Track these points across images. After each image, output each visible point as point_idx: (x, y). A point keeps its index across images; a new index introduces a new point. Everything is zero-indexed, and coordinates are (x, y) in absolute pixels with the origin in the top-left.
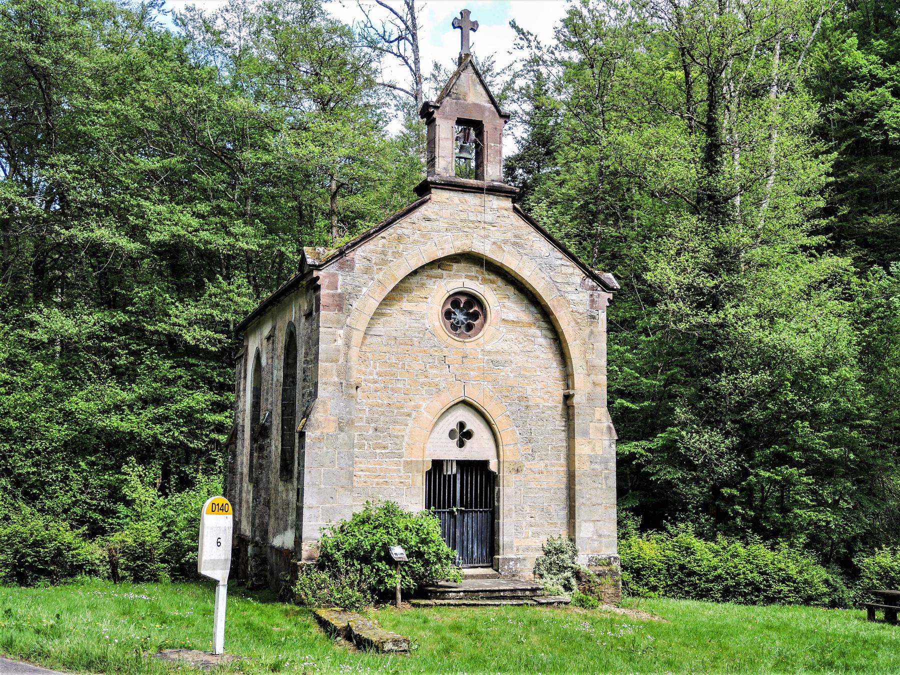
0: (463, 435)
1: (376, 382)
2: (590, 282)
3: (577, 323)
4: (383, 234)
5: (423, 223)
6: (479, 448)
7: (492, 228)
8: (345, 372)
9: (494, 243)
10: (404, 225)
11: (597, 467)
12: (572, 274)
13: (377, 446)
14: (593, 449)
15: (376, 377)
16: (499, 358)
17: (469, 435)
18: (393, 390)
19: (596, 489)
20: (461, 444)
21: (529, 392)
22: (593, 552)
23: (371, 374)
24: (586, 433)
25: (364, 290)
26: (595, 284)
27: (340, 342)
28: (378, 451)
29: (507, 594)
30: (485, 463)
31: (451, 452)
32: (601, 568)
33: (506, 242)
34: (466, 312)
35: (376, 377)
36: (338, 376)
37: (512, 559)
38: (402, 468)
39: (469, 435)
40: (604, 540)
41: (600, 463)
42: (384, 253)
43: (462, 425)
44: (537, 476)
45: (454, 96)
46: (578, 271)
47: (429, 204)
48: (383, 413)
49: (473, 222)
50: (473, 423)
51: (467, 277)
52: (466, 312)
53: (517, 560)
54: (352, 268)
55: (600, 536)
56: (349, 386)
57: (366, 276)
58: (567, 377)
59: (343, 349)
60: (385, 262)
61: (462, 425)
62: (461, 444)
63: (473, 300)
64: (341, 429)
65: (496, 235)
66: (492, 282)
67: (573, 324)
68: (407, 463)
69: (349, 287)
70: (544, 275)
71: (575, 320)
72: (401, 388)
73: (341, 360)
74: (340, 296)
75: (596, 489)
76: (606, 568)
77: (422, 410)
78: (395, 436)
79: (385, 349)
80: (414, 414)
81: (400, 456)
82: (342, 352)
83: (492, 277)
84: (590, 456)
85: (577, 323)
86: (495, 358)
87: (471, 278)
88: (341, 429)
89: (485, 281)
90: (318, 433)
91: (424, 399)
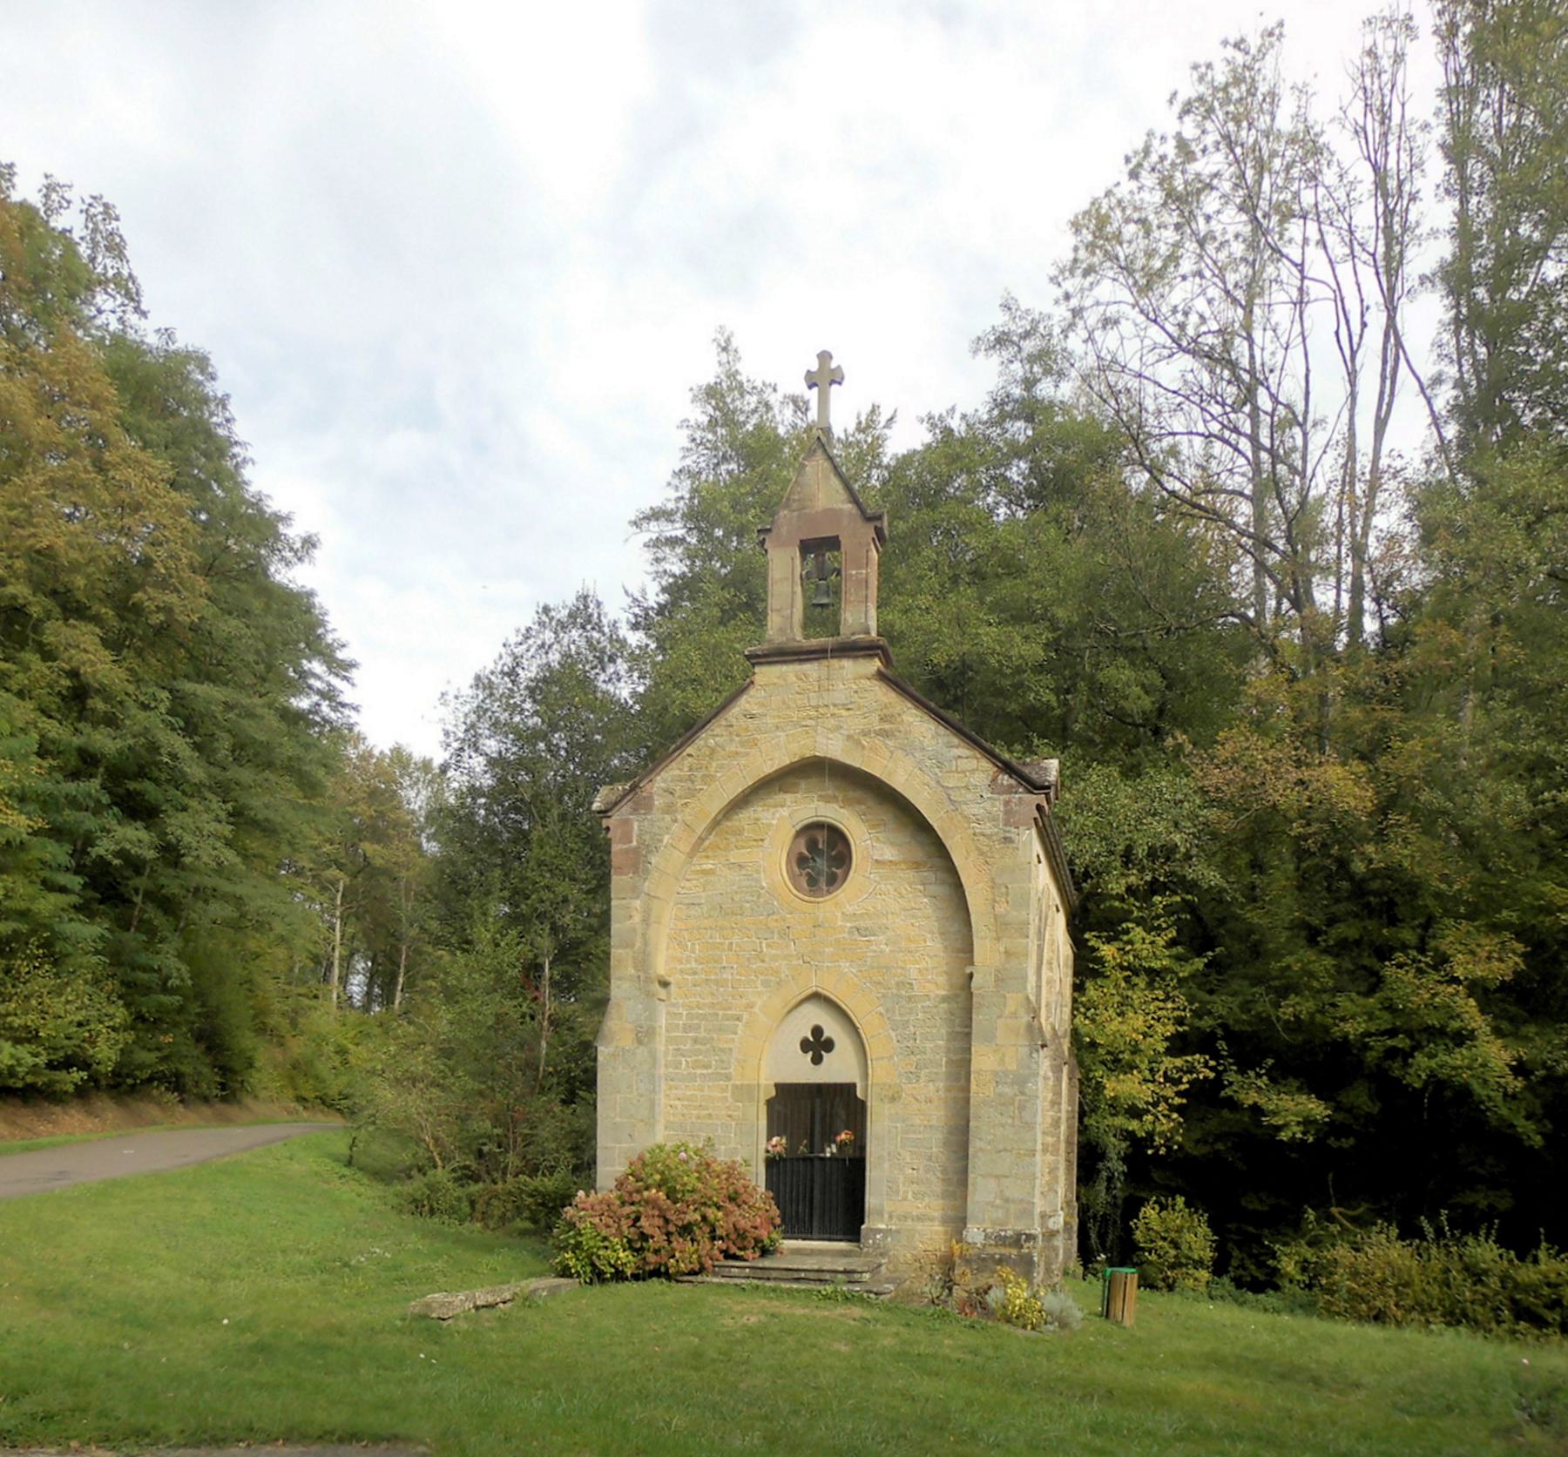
0: (817, 1045)
1: (695, 973)
2: (1005, 779)
3: (982, 853)
4: (689, 750)
5: (743, 722)
6: (837, 1068)
7: (844, 713)
8: (643, 962)
9: (849, 737)
10: (718, 731)
11: (1007, 1090)
12: (973, 771)
13: (697, 1065)
14: (1002, 1060)
15: (694, 965)
16: (869, 923)
17: (829, 1045)
18: (717, 982)
19: (1003, 1126)
20: (817, 1060)
21: (914, 974)
22: (994, 1223)
23: (688, 961)
24: (990, 1038)
25: (666, 839)
26: (1013, 782)
27: (637, 918)
28: (699, 1071)
29: (811, 1276)
30: (854, 1085)
31: (803, 1072)
32: (1003, 1251)
33: (865, 733)
34: (823, 857)
35: (694, 965)
36: (635, 967)
37: (880, 1231)
38: (729, 1095)
39: (829, 1045)
40: (1012, 1207)
41: (1013, 1084)
42: (690, 779)
43: (817, 1031)
44: (924, 1106)
45: (795, 506)
46: (986, 765)
47: (752, 691)
48: (704, 1017)
49: (816, 708)
50: (832, 1029)
51: (821, 798)
52: (823, 857)
53: (887, 1232)
54: (649, 807)
55: (1007, 1200)
56: (648, 980)
57: (668, 818)
58: (965, 949)
59: (640, 928)
60: (692, 793)
61: (817, 1031)
62: (817, 1060)
63: (837, 837)
64: (640, 1042)
65: (855, 724)
66: (859, 802)
67: (974, 854)
68: (736, 1087)
69: (647, 837)
70: (927, 779)
71: (978, 849)
72: (726, 980)
73: (638, 944)
74: (636, 850)
75: (1003, 1126)
76: (1014, 1252)
77: (756, 1010)
78: (722, 1050)
79: (706, 923)
80: (745, 1016)
81: (728, 1078)
82: (639, 932)
83: (858, 794)
84: (995, 1073)
85: (982, 853)
86: (862, 924)
87: (827, 800)
88: (640, 1042)
89: (847, 803)
90: (611, 1049)
91: (759, 994)
